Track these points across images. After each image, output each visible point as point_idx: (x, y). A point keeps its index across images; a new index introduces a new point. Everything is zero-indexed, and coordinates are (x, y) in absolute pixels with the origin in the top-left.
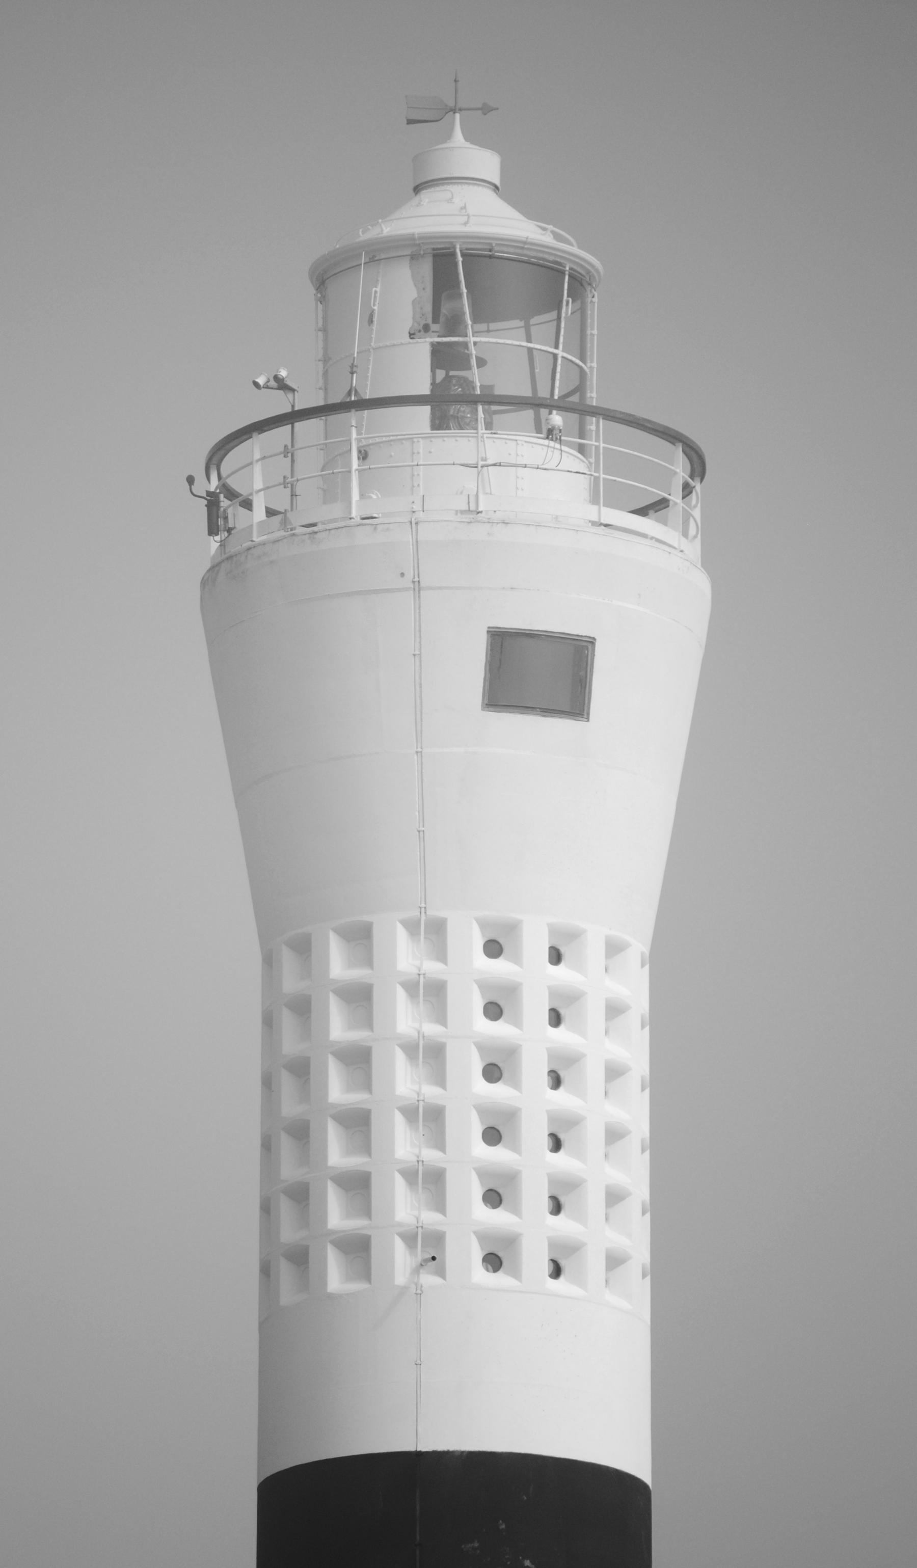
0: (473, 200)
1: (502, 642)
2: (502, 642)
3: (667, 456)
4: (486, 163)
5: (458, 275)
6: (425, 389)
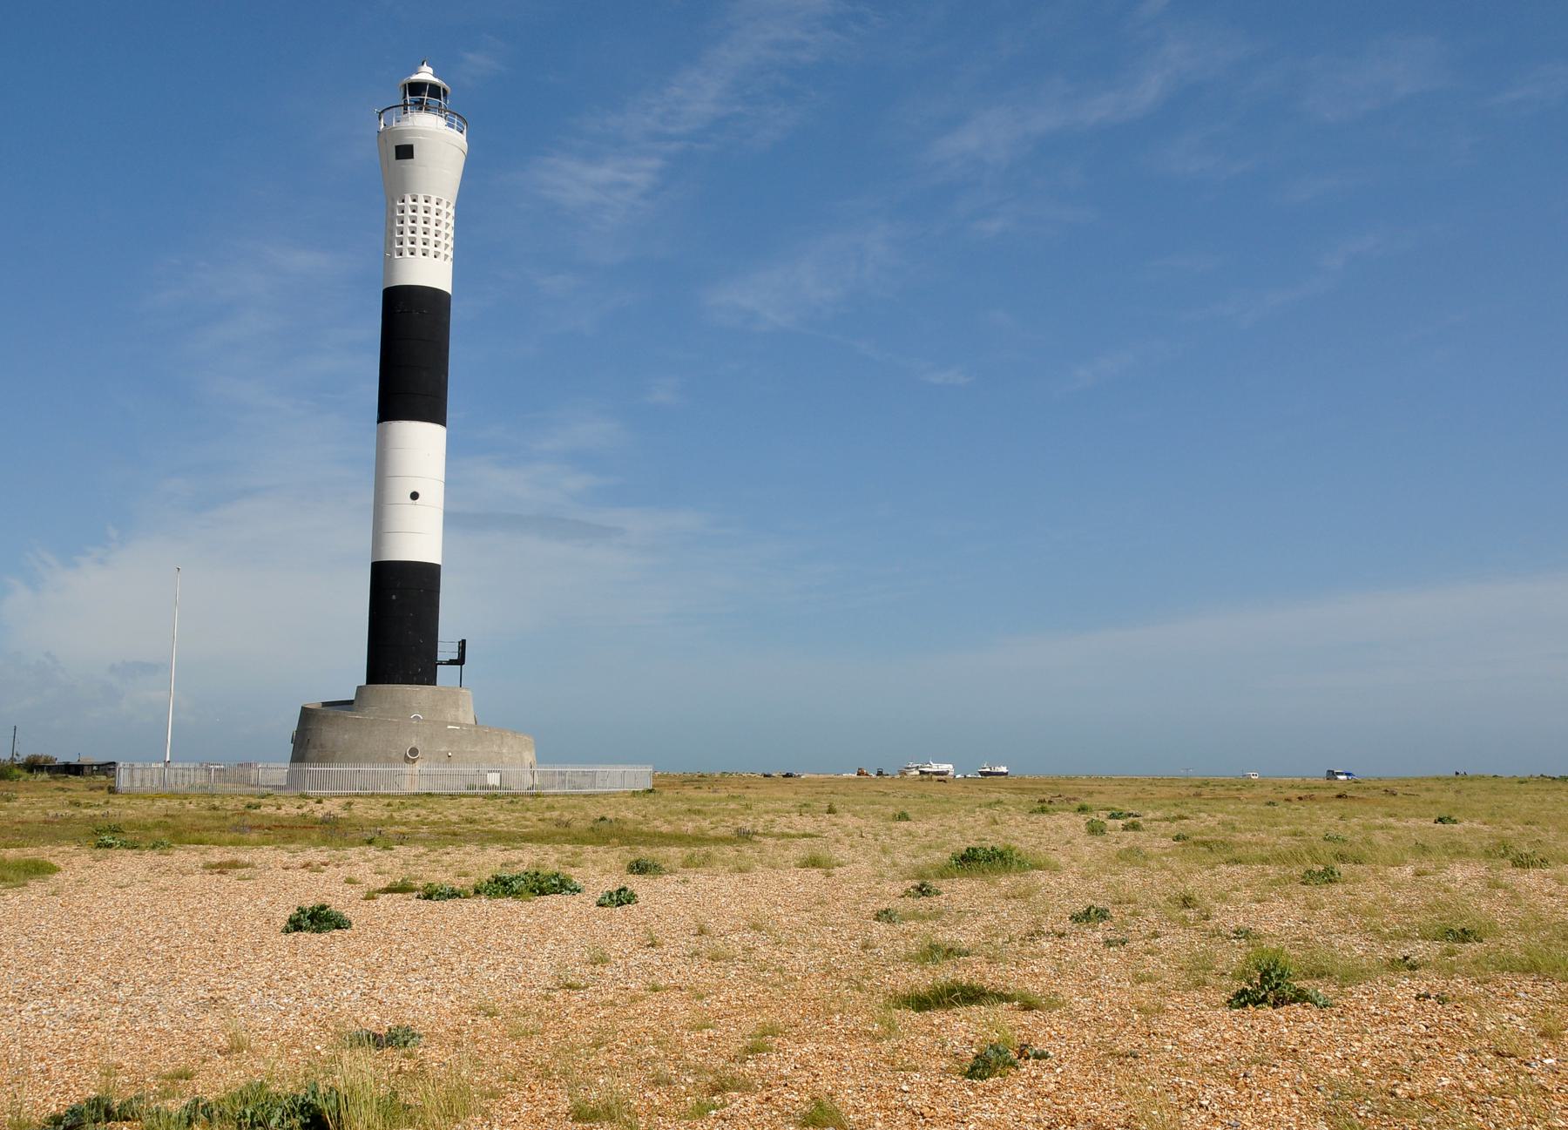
0: (426, 74)
3: (458, 117)
4: (431, 70)
5: (416, 88)
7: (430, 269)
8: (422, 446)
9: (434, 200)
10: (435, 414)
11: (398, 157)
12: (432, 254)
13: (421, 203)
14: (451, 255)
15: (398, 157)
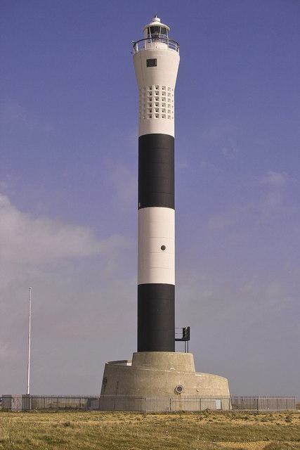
0: (157, 22)
1: (148, 61)
2: (148, 61)
4: (159, 20)
6: (181, 337)
8: (164, 219)
9: (161, 88)
12: (160, 116)
13: (161, 90)
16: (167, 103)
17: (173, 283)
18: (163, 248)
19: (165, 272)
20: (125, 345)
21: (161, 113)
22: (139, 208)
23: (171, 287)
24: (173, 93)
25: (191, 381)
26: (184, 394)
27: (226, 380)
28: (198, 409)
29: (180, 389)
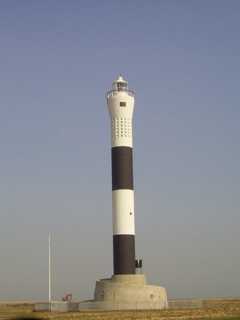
0: (121, 80)
1: (120, 103)
2: (120, 103)
3: (131, 92)
4: (122, 78)
5: (120, 84)
7: (126, 140)
8: (127, 197)
10: (131, 187)
11: (121, 106)
12: (124, 135)
13: (123, 120)
14: (131, 135)
15: (121, 106)
16: (127, 128)
17: (134, 234)
18: (131, 214)
19: (127, 227)
20: (108, 269)
21: (124, 134)
22: (113, 189)
23: (132, 237)
24: (131, 121)
25: (141, 291)
26: (155, 299)
27: (164, 288)
28: (134, 308)
29: (152, 296)
